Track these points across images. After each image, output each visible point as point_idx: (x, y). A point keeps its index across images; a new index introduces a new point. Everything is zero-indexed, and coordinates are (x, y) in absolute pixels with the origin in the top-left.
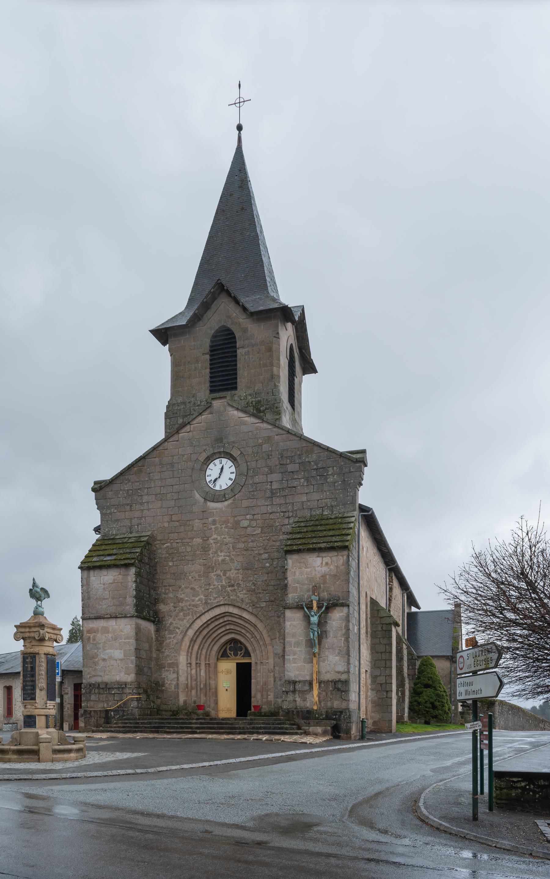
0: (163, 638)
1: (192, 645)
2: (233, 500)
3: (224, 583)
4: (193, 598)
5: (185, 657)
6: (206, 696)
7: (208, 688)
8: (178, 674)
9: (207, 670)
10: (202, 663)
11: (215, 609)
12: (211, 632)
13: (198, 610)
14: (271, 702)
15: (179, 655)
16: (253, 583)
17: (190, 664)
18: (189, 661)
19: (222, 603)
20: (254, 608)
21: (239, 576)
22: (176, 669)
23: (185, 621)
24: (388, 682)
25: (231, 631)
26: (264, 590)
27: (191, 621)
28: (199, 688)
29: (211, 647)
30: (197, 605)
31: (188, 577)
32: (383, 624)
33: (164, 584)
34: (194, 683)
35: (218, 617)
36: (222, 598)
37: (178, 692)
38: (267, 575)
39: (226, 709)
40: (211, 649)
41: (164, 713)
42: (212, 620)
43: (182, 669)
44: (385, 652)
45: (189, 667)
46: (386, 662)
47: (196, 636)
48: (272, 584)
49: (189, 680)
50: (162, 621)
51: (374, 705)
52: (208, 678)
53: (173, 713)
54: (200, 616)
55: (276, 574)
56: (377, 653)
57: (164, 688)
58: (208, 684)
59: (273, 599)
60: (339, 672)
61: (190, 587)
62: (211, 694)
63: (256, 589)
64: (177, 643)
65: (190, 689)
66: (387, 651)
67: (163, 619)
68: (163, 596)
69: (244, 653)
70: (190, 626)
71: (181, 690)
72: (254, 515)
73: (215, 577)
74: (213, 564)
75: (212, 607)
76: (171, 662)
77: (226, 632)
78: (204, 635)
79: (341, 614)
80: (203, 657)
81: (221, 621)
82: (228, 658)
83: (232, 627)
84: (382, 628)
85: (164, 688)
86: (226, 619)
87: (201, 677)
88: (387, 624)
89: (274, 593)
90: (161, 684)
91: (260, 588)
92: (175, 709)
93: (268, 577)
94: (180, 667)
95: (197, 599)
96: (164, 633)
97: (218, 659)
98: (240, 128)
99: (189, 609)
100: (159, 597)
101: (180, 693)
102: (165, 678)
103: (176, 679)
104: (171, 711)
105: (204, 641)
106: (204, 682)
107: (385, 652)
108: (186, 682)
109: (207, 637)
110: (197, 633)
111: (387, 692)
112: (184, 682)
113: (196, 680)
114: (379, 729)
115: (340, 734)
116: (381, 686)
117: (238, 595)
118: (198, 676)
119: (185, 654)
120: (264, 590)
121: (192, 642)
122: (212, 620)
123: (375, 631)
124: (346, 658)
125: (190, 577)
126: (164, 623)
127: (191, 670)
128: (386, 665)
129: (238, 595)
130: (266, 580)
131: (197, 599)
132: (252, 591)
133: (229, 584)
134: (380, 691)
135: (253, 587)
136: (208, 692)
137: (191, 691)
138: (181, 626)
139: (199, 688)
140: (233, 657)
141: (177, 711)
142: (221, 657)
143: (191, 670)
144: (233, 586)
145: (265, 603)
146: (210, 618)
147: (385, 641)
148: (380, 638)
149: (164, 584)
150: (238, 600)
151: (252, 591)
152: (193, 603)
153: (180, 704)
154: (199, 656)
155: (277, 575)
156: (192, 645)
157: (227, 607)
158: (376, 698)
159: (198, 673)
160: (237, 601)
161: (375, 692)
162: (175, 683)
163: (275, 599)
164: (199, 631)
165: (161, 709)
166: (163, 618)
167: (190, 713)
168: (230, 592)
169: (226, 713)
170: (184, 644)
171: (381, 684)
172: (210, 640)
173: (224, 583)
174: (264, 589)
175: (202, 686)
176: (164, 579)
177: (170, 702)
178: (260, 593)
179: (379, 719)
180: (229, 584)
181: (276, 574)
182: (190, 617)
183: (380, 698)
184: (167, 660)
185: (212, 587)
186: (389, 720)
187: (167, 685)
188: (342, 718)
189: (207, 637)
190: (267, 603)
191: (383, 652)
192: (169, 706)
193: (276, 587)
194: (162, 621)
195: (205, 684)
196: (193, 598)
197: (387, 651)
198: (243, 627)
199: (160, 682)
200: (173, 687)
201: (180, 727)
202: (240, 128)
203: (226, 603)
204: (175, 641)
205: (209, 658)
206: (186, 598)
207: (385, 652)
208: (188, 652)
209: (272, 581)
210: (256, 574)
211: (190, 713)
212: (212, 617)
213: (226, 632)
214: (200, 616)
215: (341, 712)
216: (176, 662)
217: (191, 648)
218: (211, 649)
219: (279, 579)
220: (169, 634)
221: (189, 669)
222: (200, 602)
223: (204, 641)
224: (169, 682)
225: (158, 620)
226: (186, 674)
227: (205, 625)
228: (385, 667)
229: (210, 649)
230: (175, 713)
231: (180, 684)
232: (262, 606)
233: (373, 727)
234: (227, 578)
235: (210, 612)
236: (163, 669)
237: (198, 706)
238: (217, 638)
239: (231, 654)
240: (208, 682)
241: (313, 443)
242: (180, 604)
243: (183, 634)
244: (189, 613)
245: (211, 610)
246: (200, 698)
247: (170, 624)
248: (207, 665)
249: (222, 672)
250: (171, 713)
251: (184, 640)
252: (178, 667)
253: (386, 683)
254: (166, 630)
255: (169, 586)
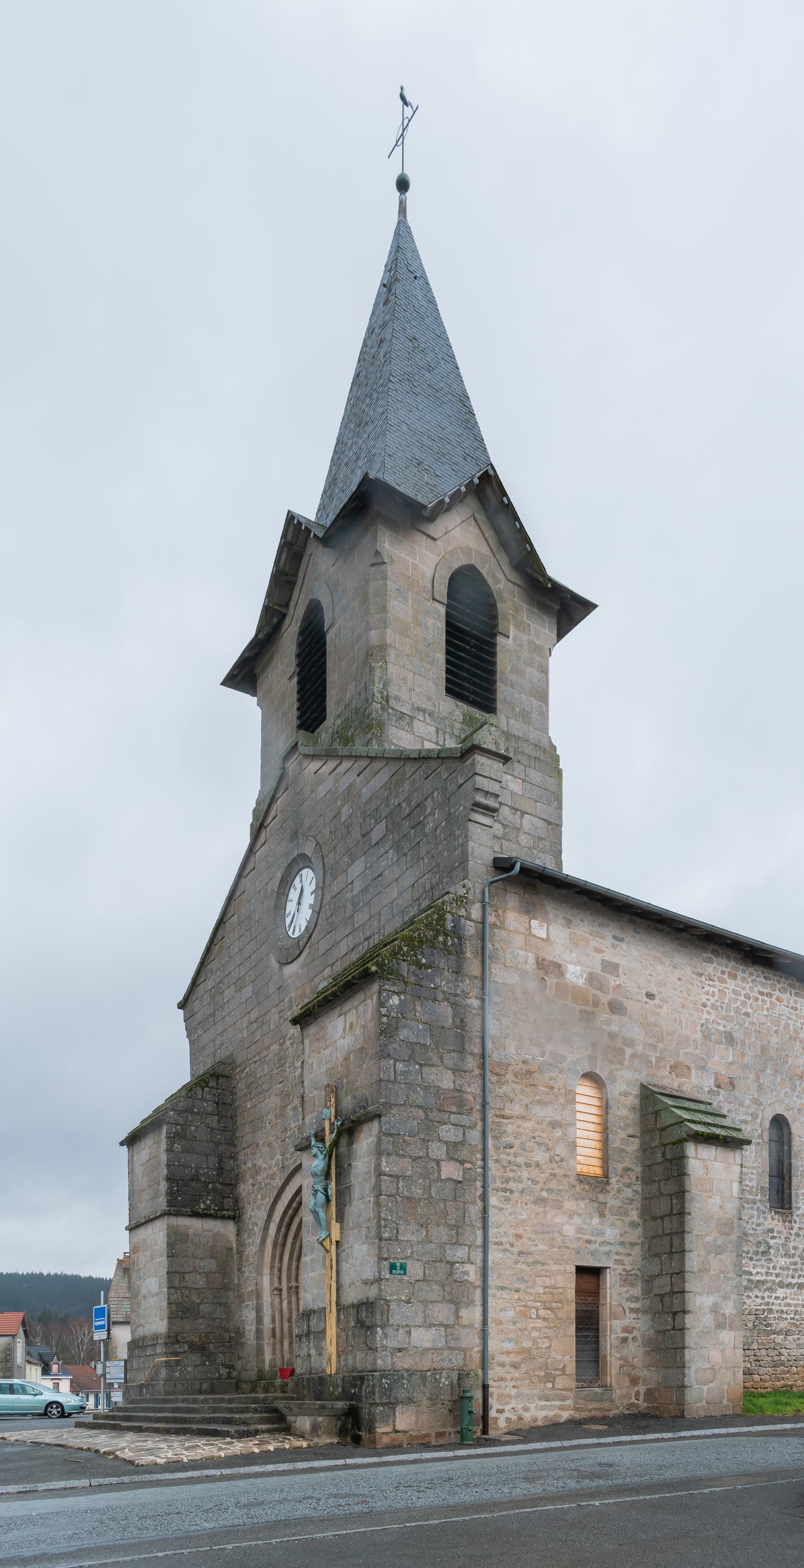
1: (278, 1253)
2: (310, 948)
18: (276, 1285)
24: (676, 1290)
32: (665, 1145)
44: (670, 1215)
46: (671, 1239)
51: (648, 1349)
56: (654, 1218)
60: (366, 1282)
66: (675, 1211)
72: (333, 964)
74: (290, 1088)
79: (370, 1140)
84: (663, 1155)
88: (673, 1144)
98: (403, 185)
107: (669, 1215)
111: (675, 1314)
114: (657, 1408)
115: (361, 1433)
116: (662, 1301)
123: (650, 1166)
124: (376, 1246)
128: (672, 1247)
134: (659, 1313)
147: (670, 1187)
148: (659, 1181)
158: (652, 1332)
161: (650, 1316)
171: (662, 1296)
179: (659, 1384)
183: (659, 1332)
186: (678, 1387)
188: (364, 1393)
191: (666, 1216)
197: (675, 1211)
202: (403, 185)
207: (669, 1215)
215: (362, 1379)
221: (277, 1300)
228: (671, 1252)
233: (645, 1404)
241: (438, 757)
253: (672, 1293)
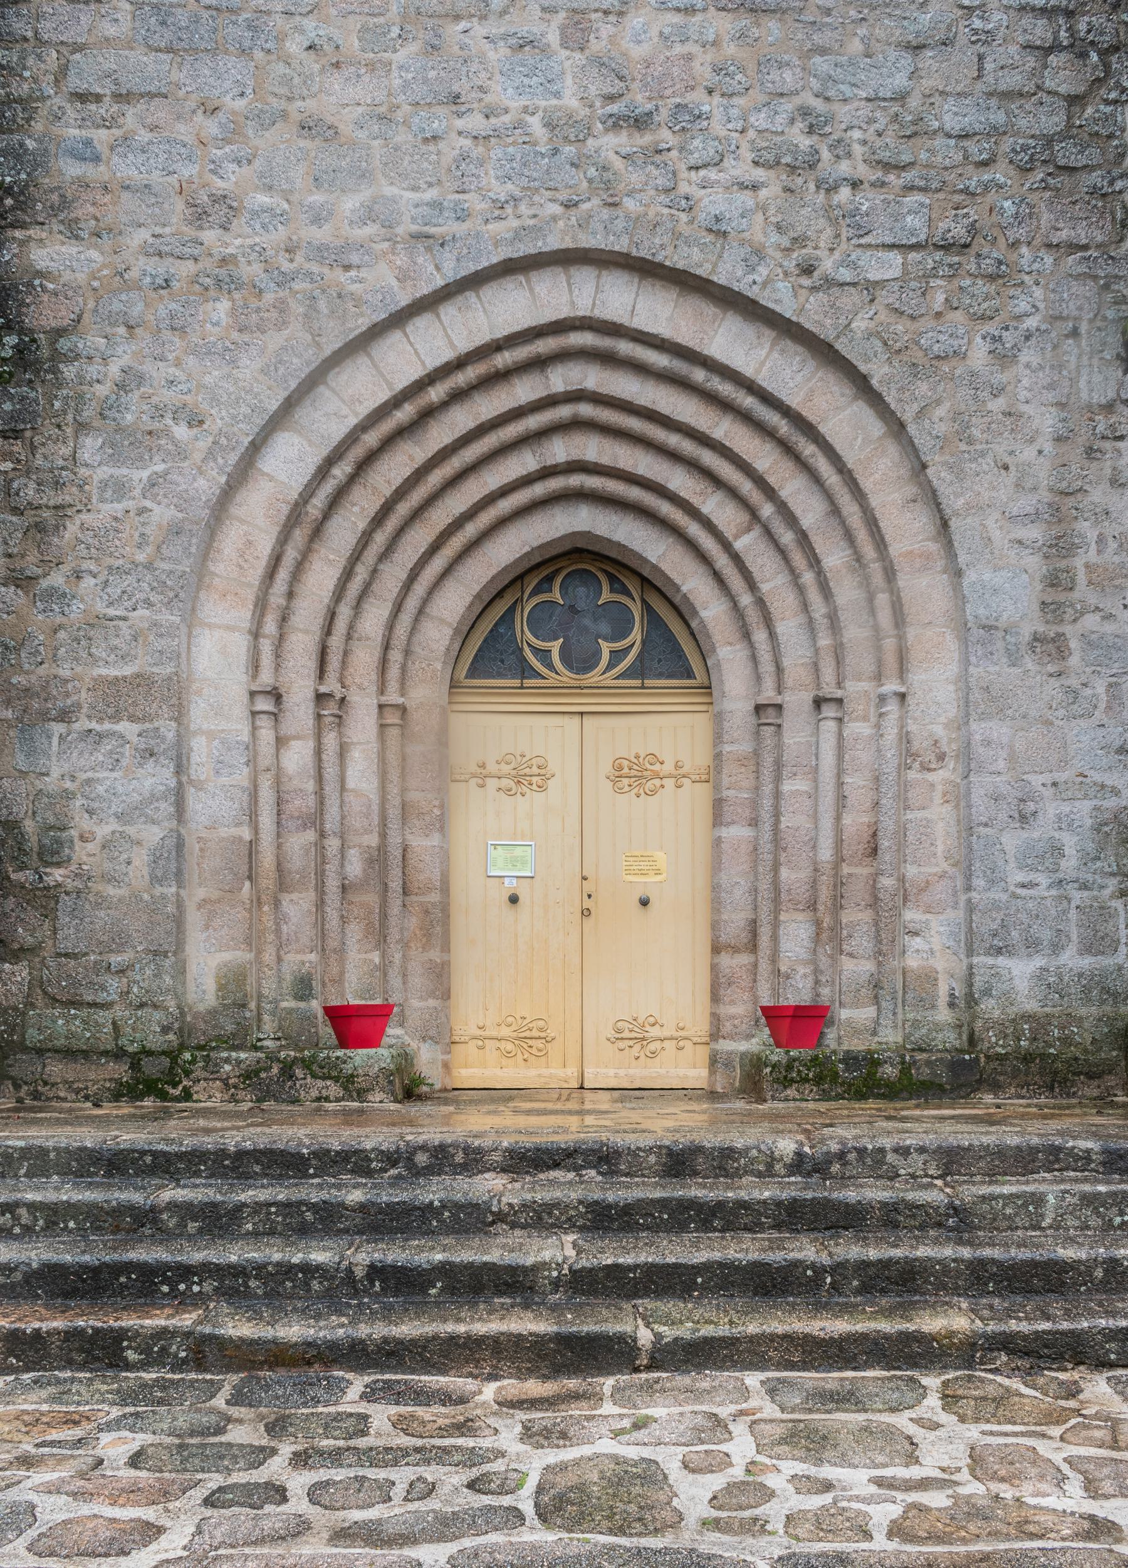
0: (58, 485)
1: (291, 555)
3: (571, 101)
4: (317, 198)
5: (240, 644)
6: (380, 935)
7: (395, 885)
8: (180, 768)
9: (392, 758)
10: (354, 697)
11: (489, 292)
12: (436, 478)
13: (355, 287)
14: (930, 978)
15: (191, 619)
16: (805, 112)
17: (276, 695)
18: (266, 678)
19: (553, 242)
20: (814, 289)
21: (689, 58)
22: (169, 730)
23: (249, 366)
25: (575, 480)
26: (887, 166)
27: (300, 366)
28: (332, 884)
29: (420, 588)
30: (347, 246)
31: (280, 38)
33: (74, 82)
34: (299, 842)
35: (504, 359)
36: (557, 209)
37: (180, 905)
38: (907, 61)
39: (505, 1032)
40: (421, 612)
41: (56, 1069)
42: (461, 379)
43: (211, 735)
45: (264, 722)
47: (328, 488)
48: (951, 123)
49: (267, 821)
50: (57, 356)
52: (393, 813)
53: (135, 1066)
54: (377, 331)
55: (981, 58)
57: (57, 875)
58: (396, 853)
59: (959, 231)
61: (295, 116)
62: (413, 922)
63: (825, 154)
64: (176, 530)
65: (267, 882)
67: (64, 344)
68: (72, 169)
69: (643, 642)
70: (289, 405)
71: (201, 893)
73: (497, 55)
75: (471, 267)
76: (128, 671)
77: (539, 490)
78: (388, 491)
80: (365, 658)
81: (524, 390)
82: (528, 682)
83: (592, 448)
85: (57, 875)
86: (559, 379)
87: (349, 798)
89: (966, 191)
90: (33, 843)
91: (858, 150)
92: (156, 1041)
93: (913, 75)
94: (198, 713)
95: (350, 204)
96: (65, 451)
97: (454, 685)
99: (284, 280)
100: (32, 181)
101: (194, 918)
102: (69, 795)
103: (166, 808)
104: (119, 1054)
105: (380, 538)
106: (373, 840)
108: (246, 834)
109: (403, 509)
110: (341, 471)
112: (224, 832)
113: (315, 820)
117: (684, 188)
118: (331, 789)
119: (244, 615)
120: (887, 166)
121: (299, 536)
122: (461, 379)
125: (294, 46)
126: (69, 371)
127: (280, 742)
129: (684, 188)
130: (901, 97)
131: (350, 204)
132: (792, 169)
133: (614, 108)
135: (805, 142)
136: (395, 909)
137: (277, 903)
138: (215, 400)
139: (332, 884)
140: (567, 677)
141: (172, 1054)
142: (473, 673)
143: (280, 742)
144: (640, 122)
145: (896, 259)
146: (447, 355)
149: (74, 82)
150: (683, 228)
151: (792, 169)
152: (320, 235)
153: (191, 997)
154: (336, 641)
155: (989, 66)
156: (291, 555)
157: (585, 278)
159: (331, 771)
160: (677, 235)
162: (153, 835)
163: (973, 230)
164: (357, 452)
165: (33, 1036)
166: (59, 332)
167: (287, 1070)
168: (618, 164)
169: (508, 1055)
170: (231, 539)
172: (420, 538)
173: (571, 101)
174: (884, 155)
175: (355, 868)
176: (78, 48)
177: (114, 984)
178: (855, 185)
180: (614, 108)
181: (981, 58)
182: (295, 329)
184: (94, 660)
185: (475, 122)
187: (83, 854)
189: (403, 509)
190: (913, 256)
192: (102, 1016)
193: (976, 149)
194: (57, 356)
195: (378, 859)
196: (317, 198)
198: (687, 447)
199: (29, 826)
200: (140, 859)
201: (375, 1271)
203: (587, 241)
204: (162, 513)
205: (404, 669)
206: (263, 199)
208: (261, 605)
209: (950, 104)
210: (823, 51)
211: (287, 1070)
212: (464, 345)
213: (539, 490)
214: (377, 331)
216: (169, 670)
217: (283, 575)
218: (421, 612)
219: (1007, 96)
220: (116, 459)
221: (266, 734)
222: (370, 230)
223: (380, 538)
224: (103, 831)
225: (19, 350)
226: (242, 776)
227: (405, 414)
229: (412, 603)
230: (152, 1068)
231: (193, 847)
232: (873, 276)
234: (599, 62)
235: (449, 311)
236: (58, 728)
237: (339, 1016)
238: (471, 530)
239: (544, 655)
240: (395, 840)
242: (209, 236)
243: (233, 458)
244: (281, 307)
245: (460, 299)
246: (341, 951)
247: (121, 387)
248: (392, 718)
249: (482, 777)
250: (121, 1071)
251: (234, 510)
252: (180, 715)
254: (82, 427)
255: (118, 97)
